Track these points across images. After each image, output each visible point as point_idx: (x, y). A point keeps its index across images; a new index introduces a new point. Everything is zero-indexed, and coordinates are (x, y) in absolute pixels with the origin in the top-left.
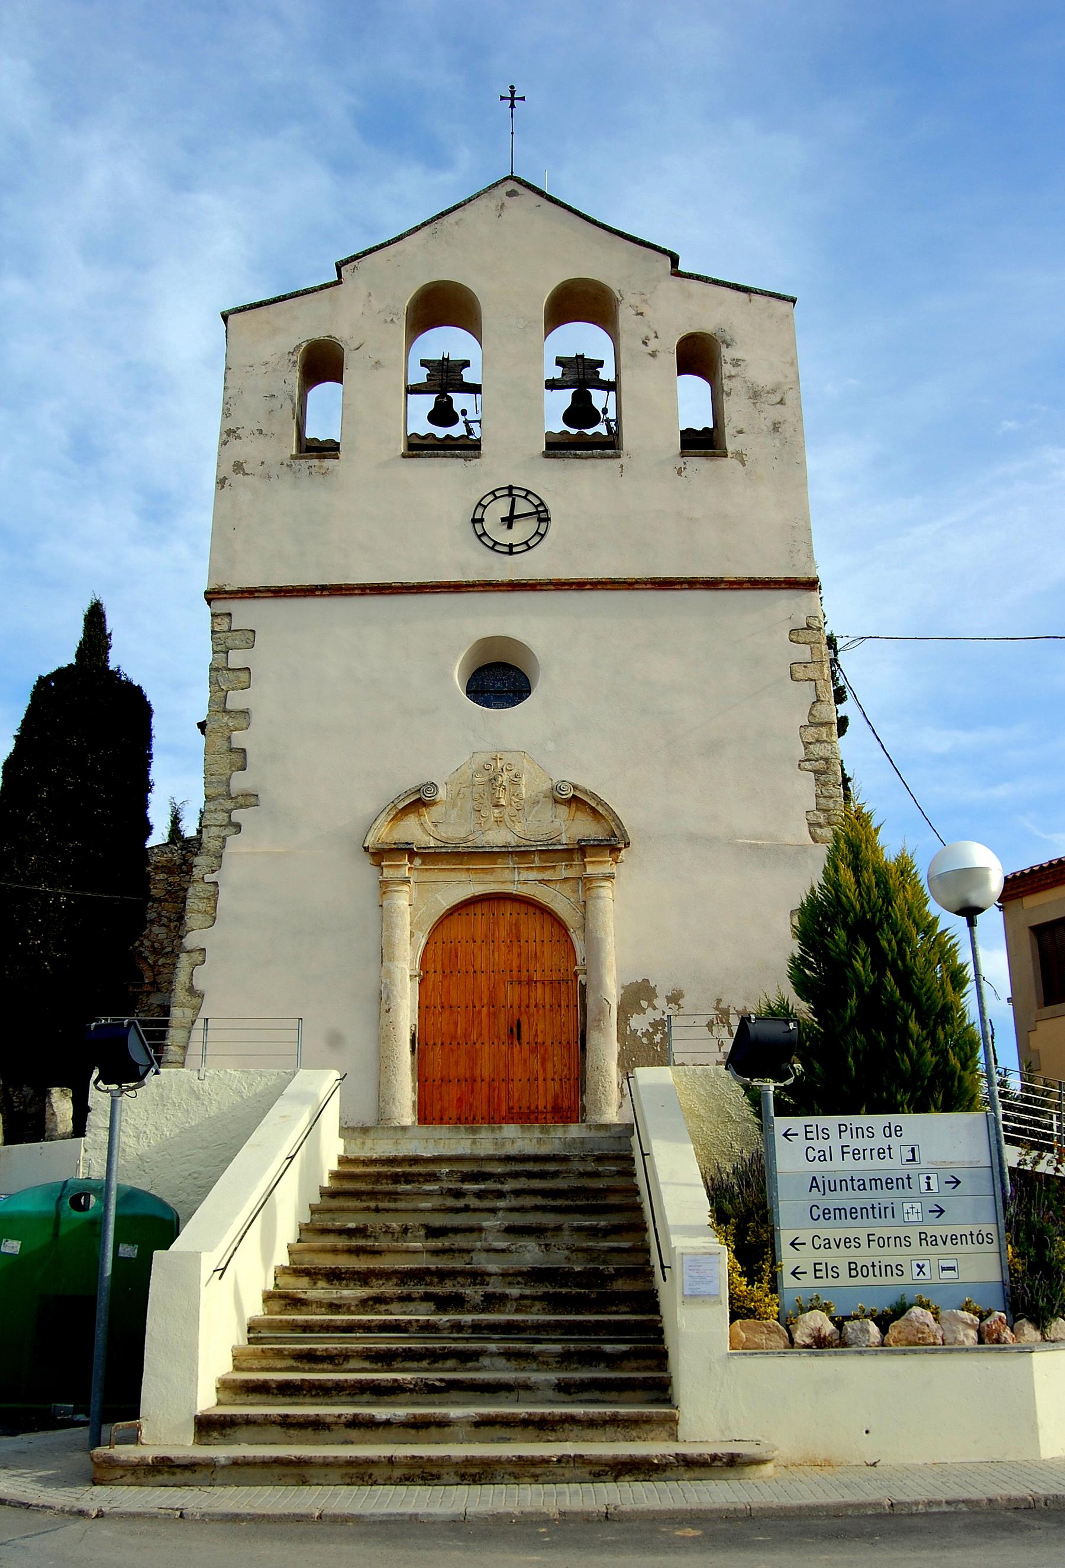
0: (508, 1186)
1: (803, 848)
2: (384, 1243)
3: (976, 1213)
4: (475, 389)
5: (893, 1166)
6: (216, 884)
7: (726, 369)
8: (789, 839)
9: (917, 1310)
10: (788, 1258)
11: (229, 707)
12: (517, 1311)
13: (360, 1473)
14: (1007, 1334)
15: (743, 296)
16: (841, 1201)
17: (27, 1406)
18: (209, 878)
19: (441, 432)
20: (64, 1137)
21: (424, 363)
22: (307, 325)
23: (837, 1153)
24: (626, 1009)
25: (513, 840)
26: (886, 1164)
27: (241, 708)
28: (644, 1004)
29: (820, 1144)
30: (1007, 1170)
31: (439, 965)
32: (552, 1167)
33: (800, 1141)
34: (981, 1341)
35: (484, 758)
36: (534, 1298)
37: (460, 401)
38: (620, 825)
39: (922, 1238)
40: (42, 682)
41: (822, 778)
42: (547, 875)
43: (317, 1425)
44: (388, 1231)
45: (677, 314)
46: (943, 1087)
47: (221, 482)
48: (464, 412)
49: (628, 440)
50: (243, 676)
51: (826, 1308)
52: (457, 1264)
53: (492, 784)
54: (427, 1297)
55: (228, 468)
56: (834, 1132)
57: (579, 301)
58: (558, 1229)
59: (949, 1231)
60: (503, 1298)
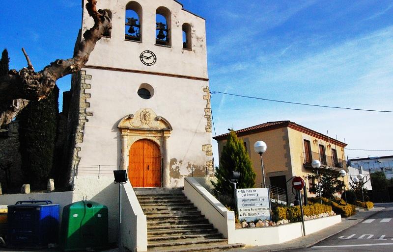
3: (266, 205)
8: (202, 131)
11: (85, 92)
12: (185, 224)
16: (249, 203)
17: (364, 245)
18: (82, 131)
29: (244, 193)
31: (133, 153)
35: (143, 110)
36: (188, 222)
40: (59, 90)
44: (150, 210)
48: (136, 31)
51: (246, 221)
52: (166, 216)
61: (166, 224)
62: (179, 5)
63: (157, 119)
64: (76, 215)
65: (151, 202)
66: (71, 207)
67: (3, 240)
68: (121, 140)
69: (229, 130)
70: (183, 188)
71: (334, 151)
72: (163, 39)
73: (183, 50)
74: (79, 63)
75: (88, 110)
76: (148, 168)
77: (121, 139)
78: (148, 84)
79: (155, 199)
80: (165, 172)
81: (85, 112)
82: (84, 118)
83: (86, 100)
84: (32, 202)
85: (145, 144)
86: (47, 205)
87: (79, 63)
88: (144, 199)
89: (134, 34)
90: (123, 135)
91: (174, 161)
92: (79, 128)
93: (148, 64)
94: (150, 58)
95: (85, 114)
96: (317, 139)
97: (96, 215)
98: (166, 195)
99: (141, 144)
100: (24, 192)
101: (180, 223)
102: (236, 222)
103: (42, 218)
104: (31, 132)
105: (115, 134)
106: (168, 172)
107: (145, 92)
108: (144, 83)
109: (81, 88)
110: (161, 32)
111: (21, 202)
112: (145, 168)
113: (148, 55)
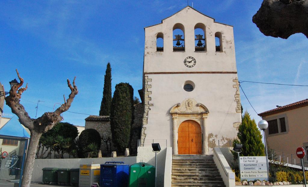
1: (235, 114)
2: (183, 171)
3: (265, 169)
5: (255, 163)
6: (147, 118)
9: (258, 181)
10: (242, 174)
11: (148, 90)
14: (269, 184)
16: (248, 167)
18: (146, 117)
19: (177, 46)
20: (128, 156)
23: (247, 161)
25: (192, 112)
27: (150, 91)
28: (212, 137)
29: (245, 160)
30: (102, 117)
31: (182, 130)
32: (203, 161)
33: (243, 160)
34: (266, 185)
35: (187, 99)
36: (207, 179)
39: (258, 172)
41: (238, 103)
44: (184, 170)
46: (259, 153)
48: (182, 44)
51: (246, 180)
52: (194, 174)
54: (193, 179)
58: (206, 170)
59: (261, 171)
60: (202, 179)
61: (190, 180)
63: (197, 105)
64: (135, 171)
65: (187, 165)
66: (132, 166)
67: (98, 184)
68: (172, 122)
69: (277, 106)
70: (212, 156)
72: (201, 47)
73: (216, 53)
74: (66, 108)
75: (150, 102)
76: (192, 140)
77: (172, 120)
78: (190, 81)
79: (191, 162)
80: (204, 143)
81: (148, 104)
82: (148, 108)
83: (148, 96)
84: (113, 162)
85: (190, 124)
86: (121, 165)
87: (66, 108)
88: (183, 162)
89: (179, 47)
90: (173, 118)
91: (211, 135)
92: (145, 115)
93: (190, 66)
94: (191, 62)
95: (148, 106)
97: (147, 172)
98: (200, 160)
99: (187, 124)
100: (113, 157)
101: (201, 179)
102: (236, 181)
103: (117, 172)
104: (116, 119)
105: (168, 118)
106: (206, 143)
108: (187, 80)
109: (146, 88)
110: (200, 41)
111: (108, 162)
112: (190, 141)
113: (190, 60)
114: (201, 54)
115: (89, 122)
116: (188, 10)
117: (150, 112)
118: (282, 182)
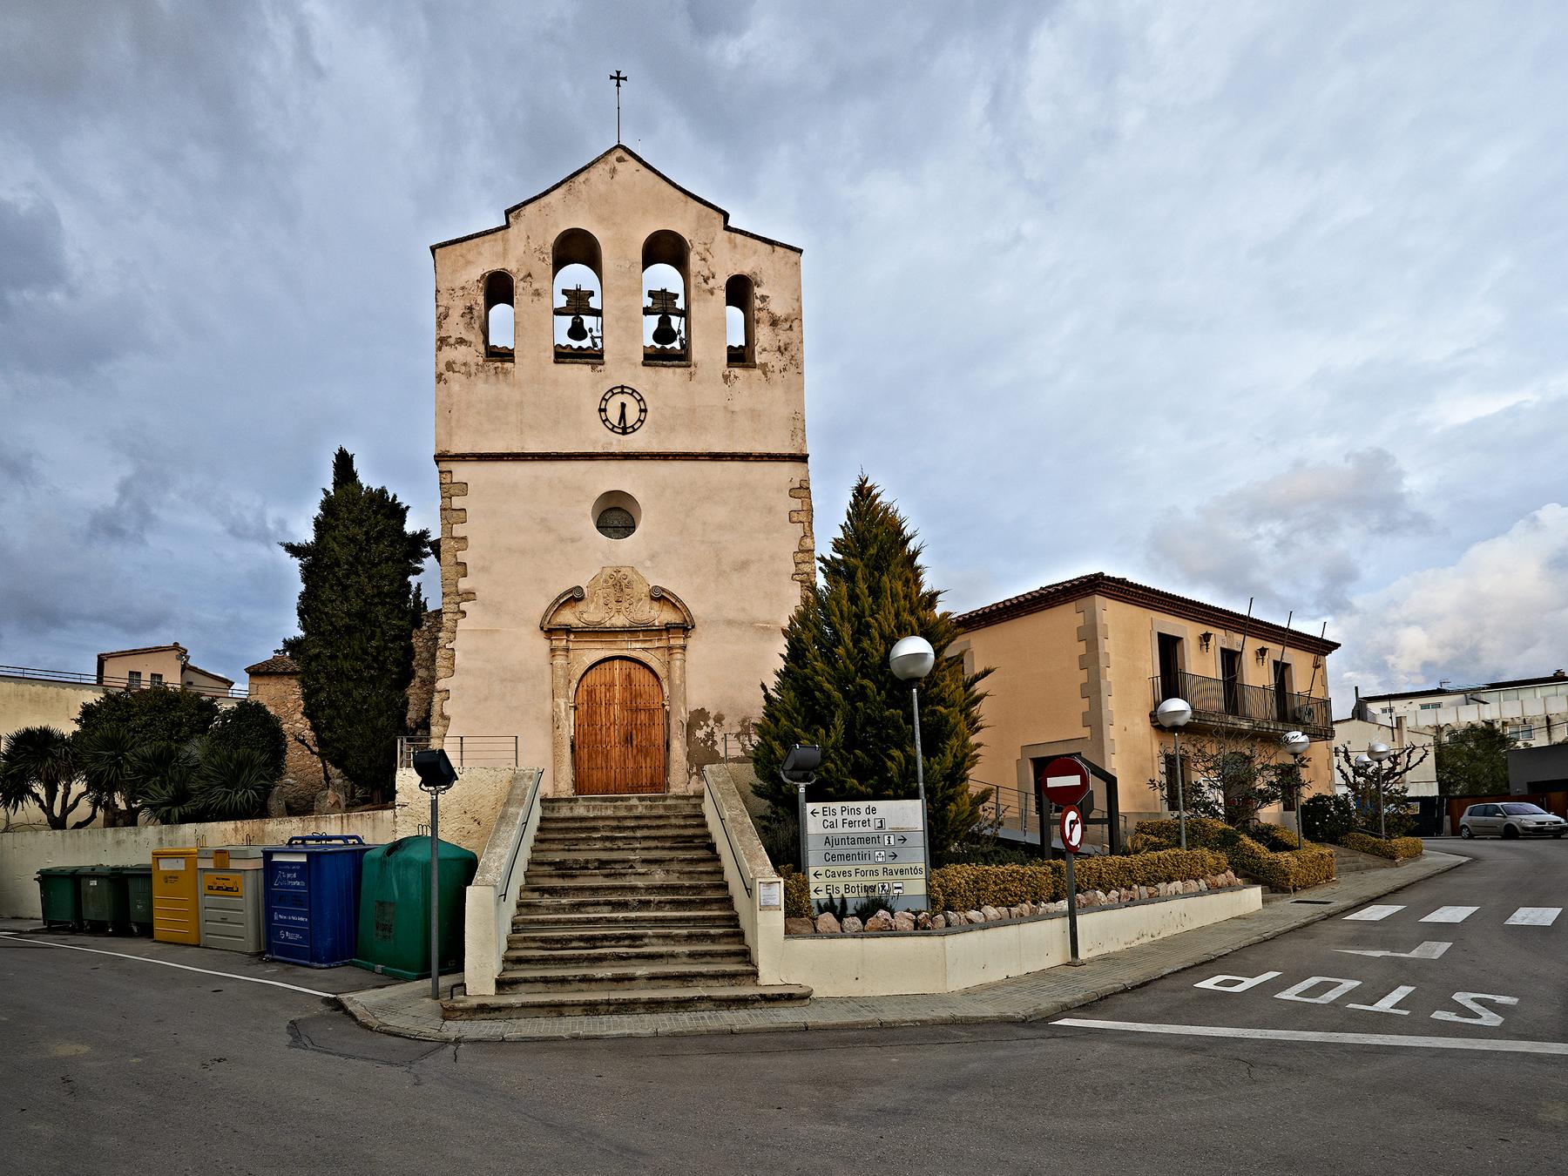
0: (639, 834)
4: (598, 313)
5: (869, 830)
7: (757, 303)
13: (591, 1008)
15: (768, 247)
16: (842, 850)
19: (575, 344)
21: (565, 292)
22: (486, 261)
24: (691, 727)
26: (865, 830)
29: (830, 818)
33: (820, 817)
35: (609, 571)
37: (589, 322)
38: (689, 614)
42: (646, 645)
43: (563, 981)
45: (725, 262)
47: (439, 377)
49: (696, 355)
50: (461, 514)
53: (619, 585)
55: (442, 367)
56: (838, 811)
57: (664, 247)
58: (671, 860)
59: (898, 867)
62: (715, 214)
71: (1281, 669)
96: (1211, 630)
107: (616, 516)
114: (670, 376)
115: (265, 681)
116: (619, 166)
117: (462, 624)
118: (979, 909)
